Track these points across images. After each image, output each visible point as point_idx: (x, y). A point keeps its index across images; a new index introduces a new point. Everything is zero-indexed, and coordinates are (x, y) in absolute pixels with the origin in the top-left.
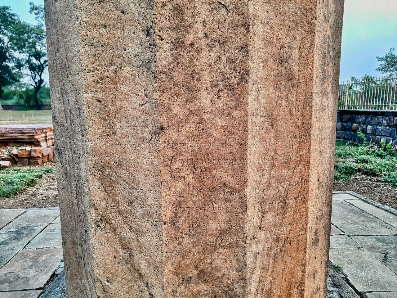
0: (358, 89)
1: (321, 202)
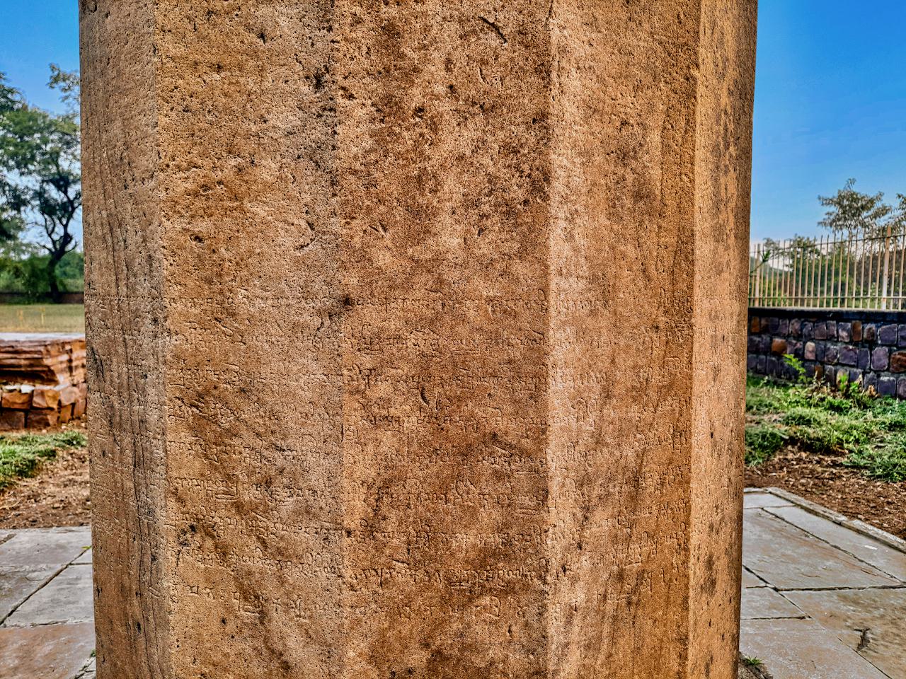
0: (779, 264)
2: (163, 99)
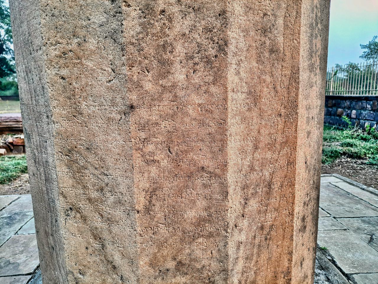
0: (342, 75)
1: (309, 186)
2: (42, 10)
